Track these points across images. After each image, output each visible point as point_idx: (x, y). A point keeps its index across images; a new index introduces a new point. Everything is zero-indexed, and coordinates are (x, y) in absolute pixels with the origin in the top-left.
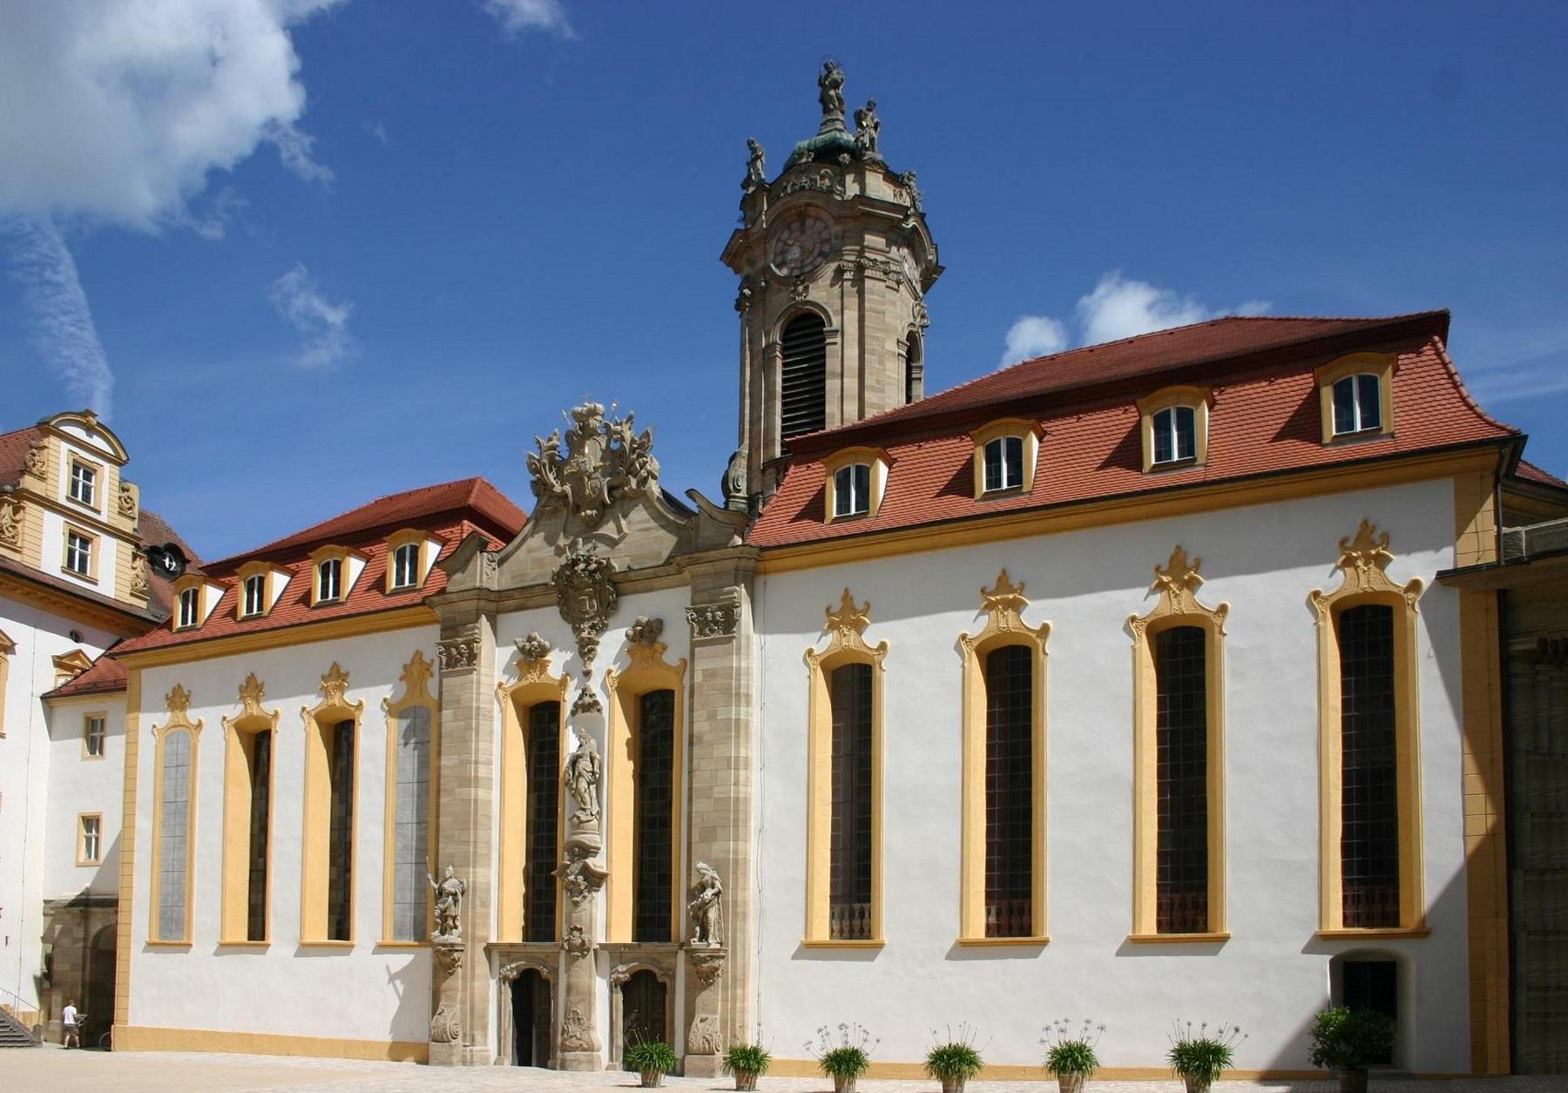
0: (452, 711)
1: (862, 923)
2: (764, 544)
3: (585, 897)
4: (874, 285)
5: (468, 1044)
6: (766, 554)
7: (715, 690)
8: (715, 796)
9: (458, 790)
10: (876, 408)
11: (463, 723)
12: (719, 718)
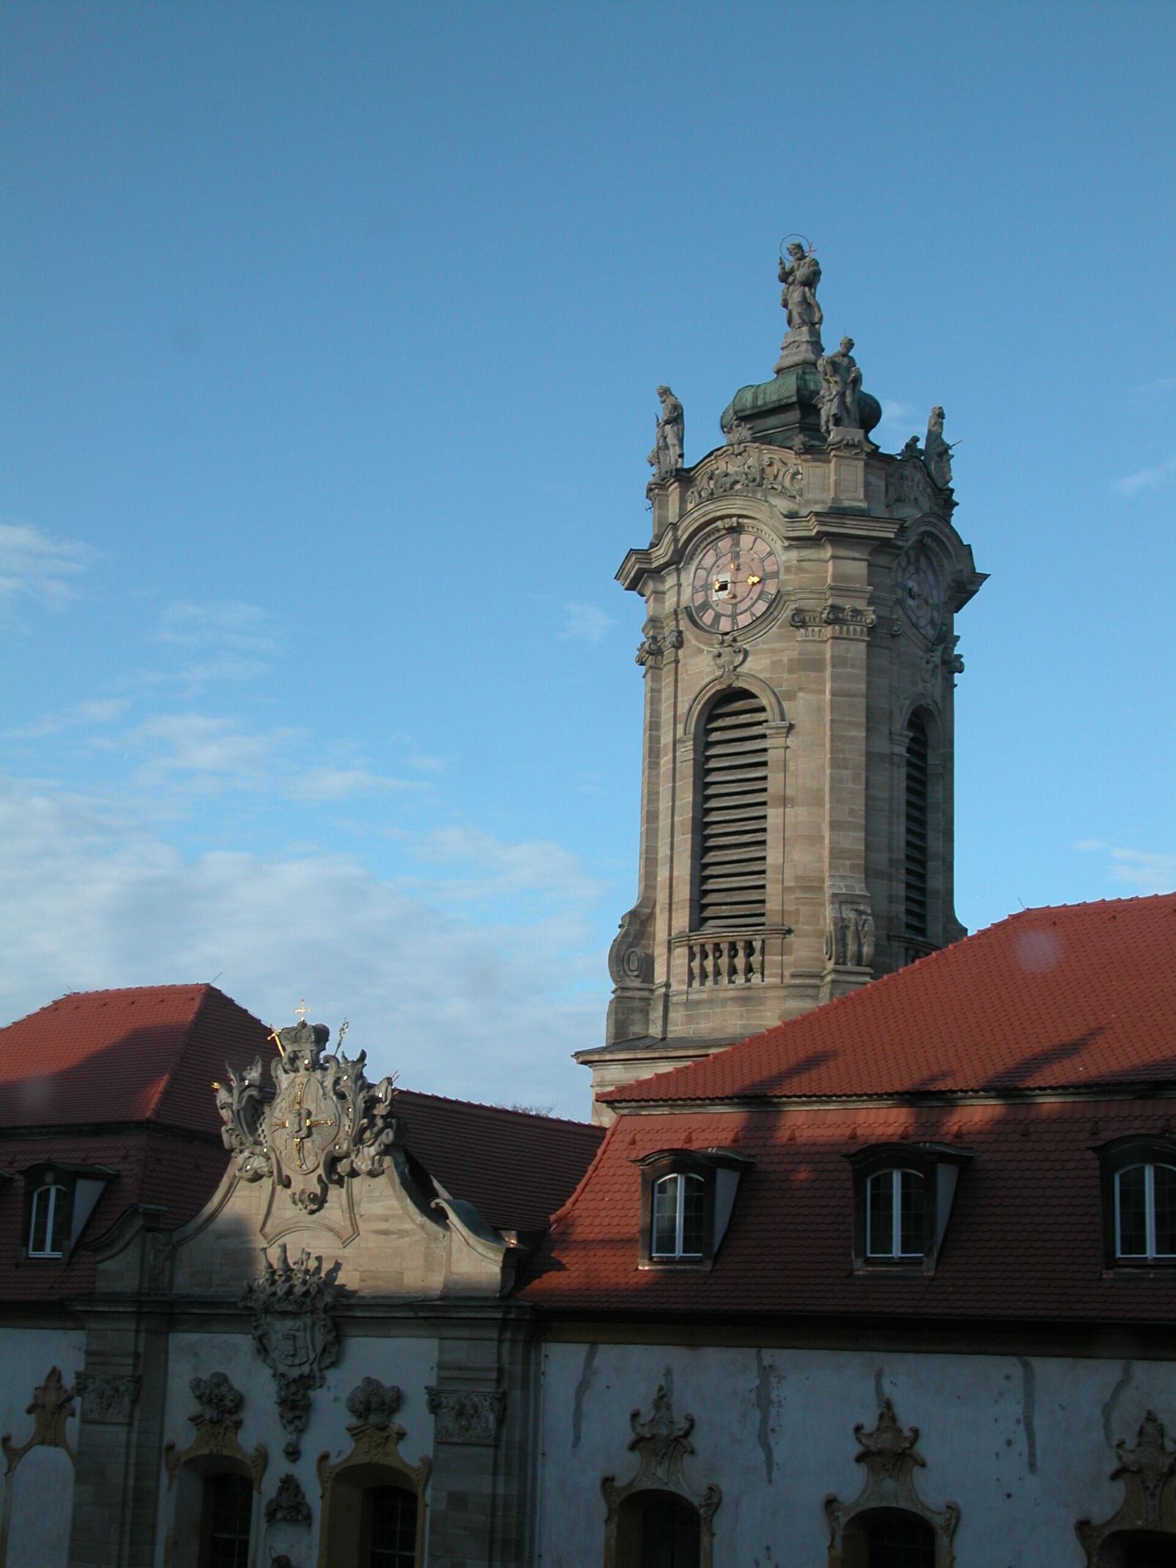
4: (848, 651)
10: (848, 859)
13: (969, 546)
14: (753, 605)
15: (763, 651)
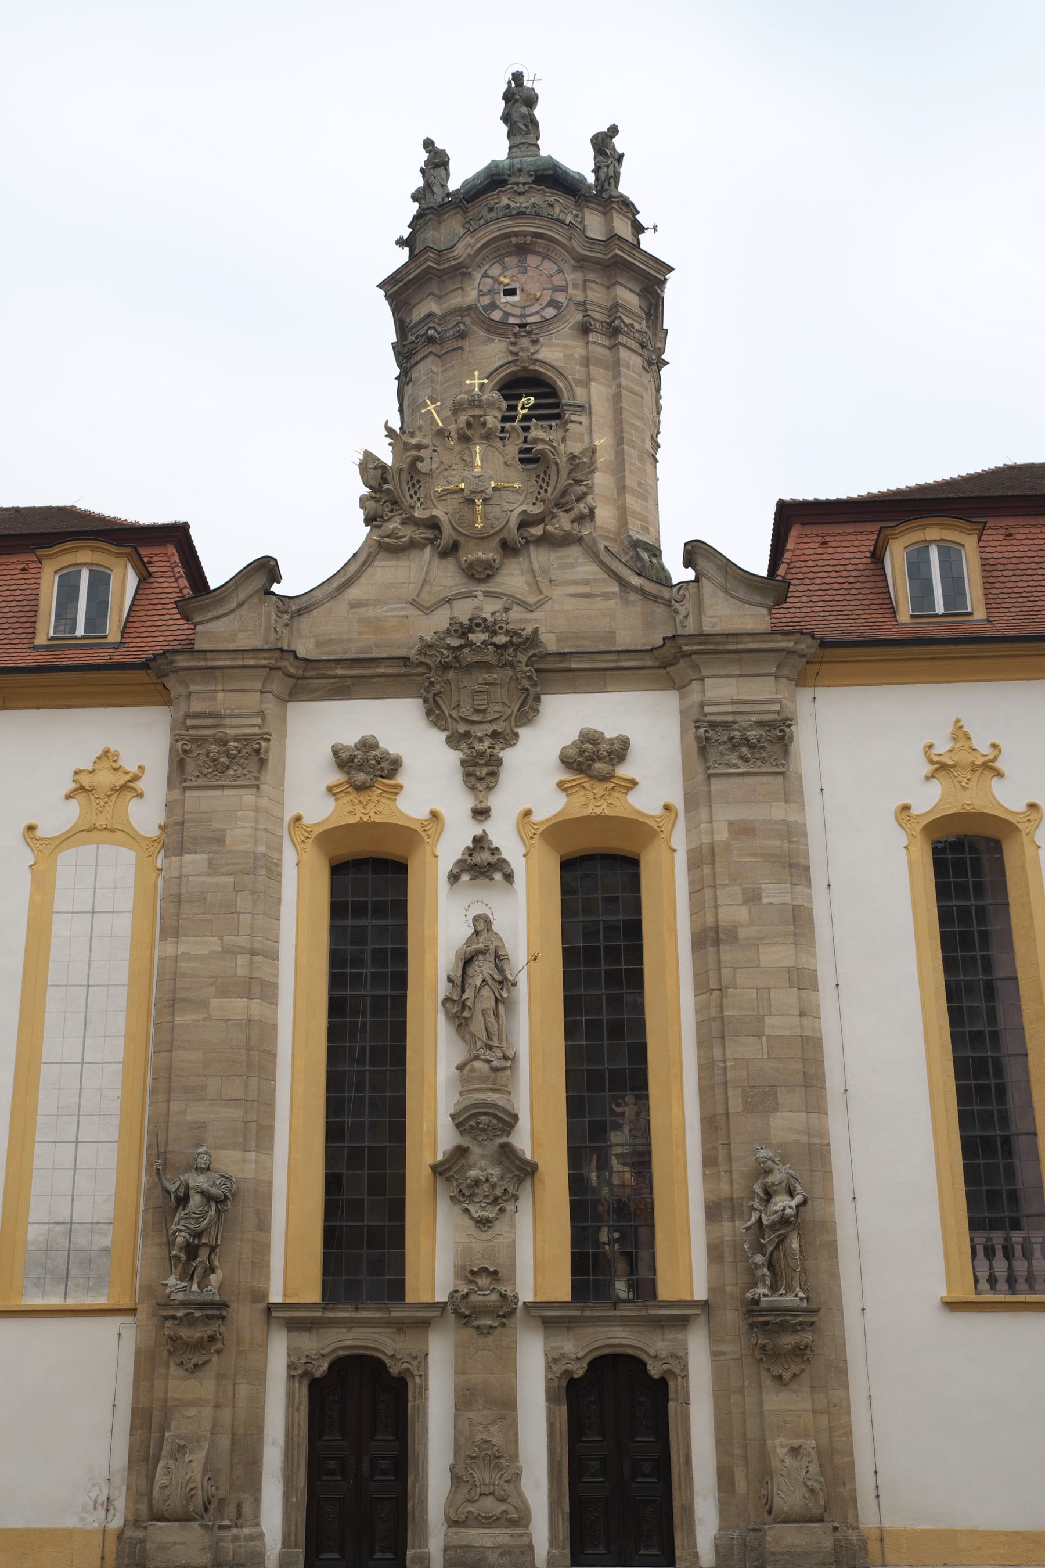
0: (206, 856)
1: (991, 1267)
2: (829, 636)
3: (502, 1211)
5: (226, 1523)
6: (829, 652)
7: (752, 855)
8: (768, 1031)
9: (214, 1003)
11: (231, 879)
12: (765, 901)
13: (667, 330)
14: (543, 309)
15: (558, 345)
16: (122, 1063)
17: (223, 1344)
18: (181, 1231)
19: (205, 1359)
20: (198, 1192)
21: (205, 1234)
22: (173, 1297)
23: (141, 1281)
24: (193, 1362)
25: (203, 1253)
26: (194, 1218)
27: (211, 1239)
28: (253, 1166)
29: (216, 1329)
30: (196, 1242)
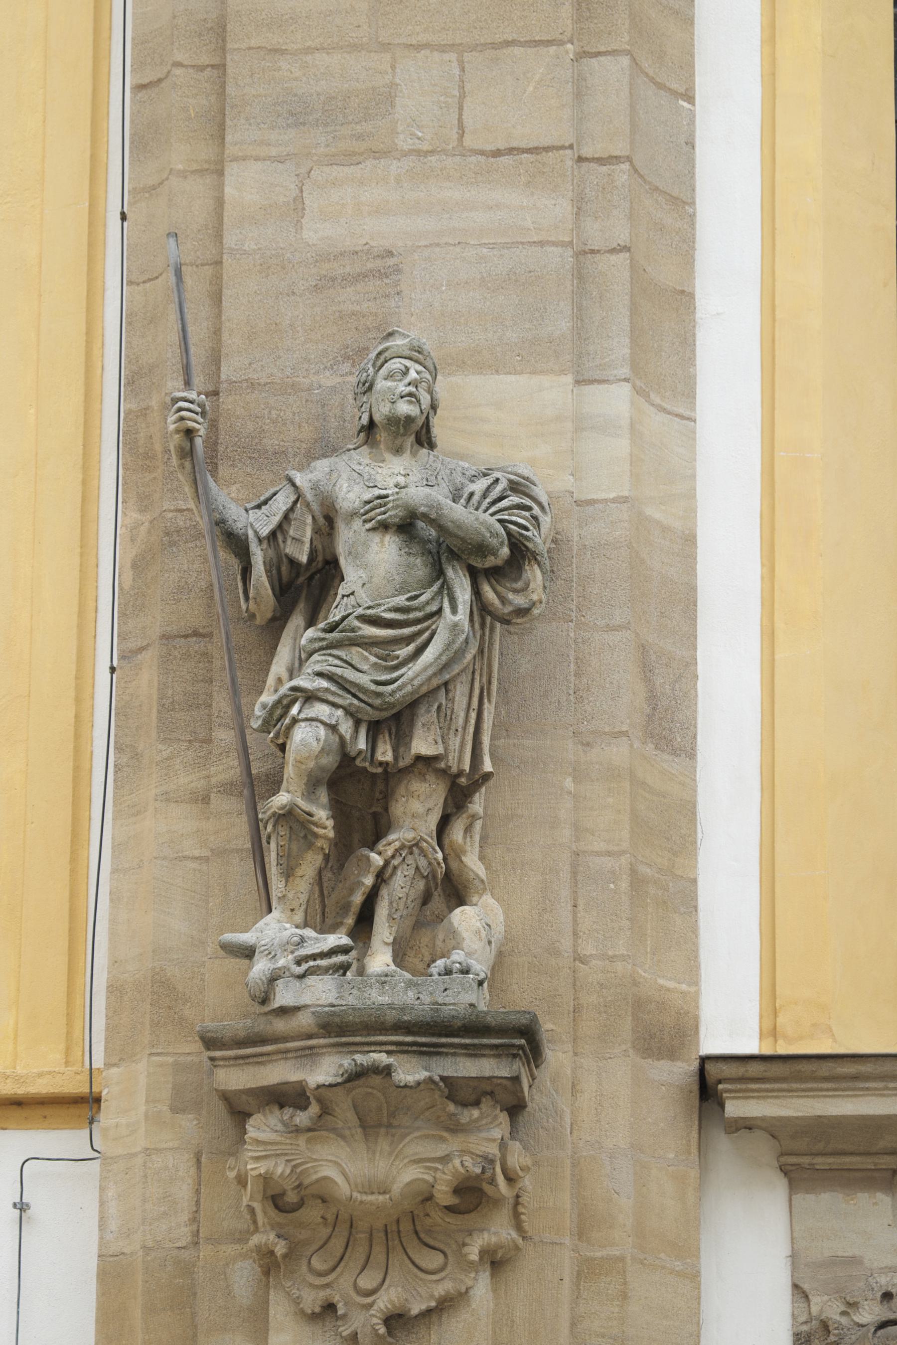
14: (199, 1226)
16: (91, 1092)
17: (519, 1227)
18: (310, 697)
19: (440, 1290)
20: (384, 527)
21: (426, 717)
22: (284, 996)
23: (114, 962)
24: (385, 1301)
25: (416, 806)
26: (368, 644)
27: (455, 742)
28: (622, 446)
29: (493, 1150)
30: (385, 753)
